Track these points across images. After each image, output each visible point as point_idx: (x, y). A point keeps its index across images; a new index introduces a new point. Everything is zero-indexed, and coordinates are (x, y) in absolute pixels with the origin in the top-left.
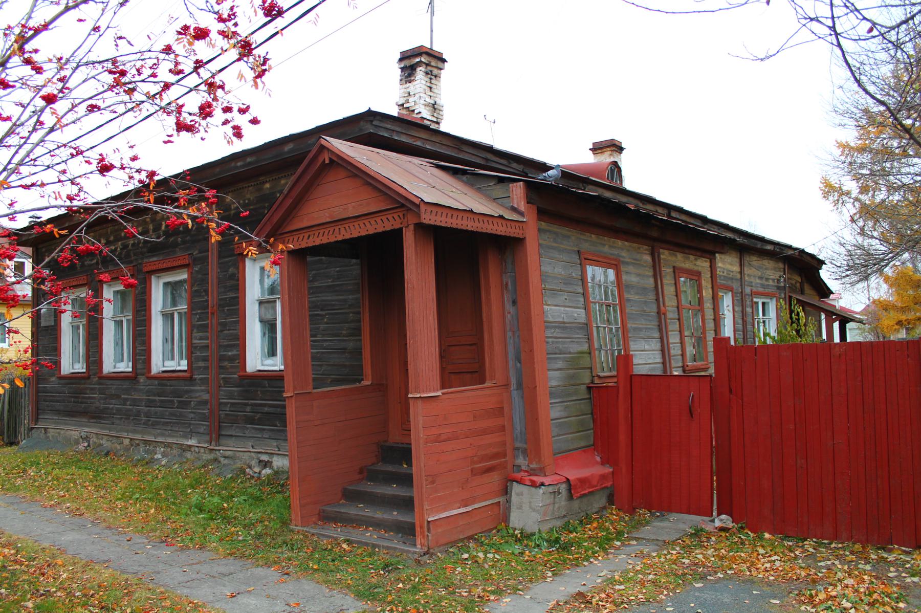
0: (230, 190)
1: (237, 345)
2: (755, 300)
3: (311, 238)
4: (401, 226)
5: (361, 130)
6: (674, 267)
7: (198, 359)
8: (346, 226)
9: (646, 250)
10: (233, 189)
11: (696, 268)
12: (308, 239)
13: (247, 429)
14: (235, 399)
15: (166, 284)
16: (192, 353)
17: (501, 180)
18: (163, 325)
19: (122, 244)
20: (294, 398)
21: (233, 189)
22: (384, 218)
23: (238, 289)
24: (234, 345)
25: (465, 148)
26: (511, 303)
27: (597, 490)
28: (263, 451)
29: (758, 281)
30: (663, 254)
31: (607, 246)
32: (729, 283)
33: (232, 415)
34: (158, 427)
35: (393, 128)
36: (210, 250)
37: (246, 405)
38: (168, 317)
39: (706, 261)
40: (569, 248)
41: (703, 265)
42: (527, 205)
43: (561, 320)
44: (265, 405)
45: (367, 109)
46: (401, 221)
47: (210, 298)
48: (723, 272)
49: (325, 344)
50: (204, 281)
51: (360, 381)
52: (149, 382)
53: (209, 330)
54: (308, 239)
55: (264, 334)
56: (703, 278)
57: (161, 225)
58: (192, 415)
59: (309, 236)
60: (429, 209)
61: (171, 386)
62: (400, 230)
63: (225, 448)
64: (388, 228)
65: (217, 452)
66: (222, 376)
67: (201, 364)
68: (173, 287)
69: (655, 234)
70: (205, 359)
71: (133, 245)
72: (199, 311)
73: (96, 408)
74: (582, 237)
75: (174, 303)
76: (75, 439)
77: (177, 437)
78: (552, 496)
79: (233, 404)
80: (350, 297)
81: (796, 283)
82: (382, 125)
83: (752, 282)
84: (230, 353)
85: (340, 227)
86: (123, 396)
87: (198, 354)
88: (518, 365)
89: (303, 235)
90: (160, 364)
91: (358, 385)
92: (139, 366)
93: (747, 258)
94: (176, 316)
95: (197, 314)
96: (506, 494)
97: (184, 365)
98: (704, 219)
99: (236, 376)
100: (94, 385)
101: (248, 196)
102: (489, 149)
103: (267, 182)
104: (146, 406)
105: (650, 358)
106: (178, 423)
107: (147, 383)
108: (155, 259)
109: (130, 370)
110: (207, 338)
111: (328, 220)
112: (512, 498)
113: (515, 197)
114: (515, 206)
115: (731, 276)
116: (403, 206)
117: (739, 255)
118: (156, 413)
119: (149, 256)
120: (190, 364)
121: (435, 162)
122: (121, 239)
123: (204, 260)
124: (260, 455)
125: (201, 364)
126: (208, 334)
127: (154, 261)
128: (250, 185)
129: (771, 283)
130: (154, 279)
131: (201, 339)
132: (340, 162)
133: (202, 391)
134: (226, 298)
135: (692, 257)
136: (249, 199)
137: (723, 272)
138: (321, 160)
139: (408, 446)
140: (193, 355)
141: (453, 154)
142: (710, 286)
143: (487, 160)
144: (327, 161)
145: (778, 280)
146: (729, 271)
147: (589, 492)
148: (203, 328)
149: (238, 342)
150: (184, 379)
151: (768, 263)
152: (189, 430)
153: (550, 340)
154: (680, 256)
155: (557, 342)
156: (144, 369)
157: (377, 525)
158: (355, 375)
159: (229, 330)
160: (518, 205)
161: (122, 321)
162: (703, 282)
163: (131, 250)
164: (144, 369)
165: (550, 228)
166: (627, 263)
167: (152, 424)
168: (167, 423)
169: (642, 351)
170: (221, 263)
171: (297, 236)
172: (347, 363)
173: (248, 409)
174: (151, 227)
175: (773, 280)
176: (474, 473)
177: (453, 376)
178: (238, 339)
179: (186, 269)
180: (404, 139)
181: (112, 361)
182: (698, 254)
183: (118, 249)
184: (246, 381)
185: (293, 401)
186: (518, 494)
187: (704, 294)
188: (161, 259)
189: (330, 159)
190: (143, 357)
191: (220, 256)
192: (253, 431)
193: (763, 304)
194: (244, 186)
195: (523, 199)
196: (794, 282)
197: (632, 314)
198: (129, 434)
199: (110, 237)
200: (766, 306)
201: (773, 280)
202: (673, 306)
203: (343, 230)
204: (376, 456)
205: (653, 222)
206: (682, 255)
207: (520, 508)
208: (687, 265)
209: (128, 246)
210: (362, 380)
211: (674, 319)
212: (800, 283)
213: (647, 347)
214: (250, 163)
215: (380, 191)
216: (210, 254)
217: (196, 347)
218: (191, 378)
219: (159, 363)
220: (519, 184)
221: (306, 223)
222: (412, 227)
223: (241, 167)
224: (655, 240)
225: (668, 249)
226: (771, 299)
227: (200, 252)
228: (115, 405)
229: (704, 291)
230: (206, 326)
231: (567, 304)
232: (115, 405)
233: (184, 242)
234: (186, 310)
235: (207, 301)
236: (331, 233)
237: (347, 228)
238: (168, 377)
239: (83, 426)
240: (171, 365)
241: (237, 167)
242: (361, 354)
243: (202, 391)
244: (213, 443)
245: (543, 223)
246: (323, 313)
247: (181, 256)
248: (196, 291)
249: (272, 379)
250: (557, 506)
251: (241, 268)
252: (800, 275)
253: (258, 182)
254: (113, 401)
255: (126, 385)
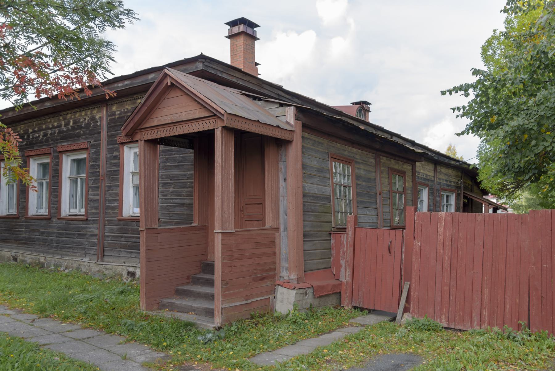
0: (115, 102)
1: (118, 200)
2: (442, 193)
3: (159, 133)
4: (214, 128)
5: (197, 67)
6: (388, 167)
7: (92, 208)
8: (181, 126)
9: (373, 156)
10: (117, 102)
11: (403, 169)
12: (157, 133)
13: (121, 251)
14: (115, 233)
15: (74, 161)
16: (88, 204)
17: (281, 105)
18: (70, 186)
19: (43, 133)
20: (145, 231)
21: (117, 102)
22: (204, 122)
23: (119, 165)
24: (116, 200)
25: (264, 86)
26: (283, 180)
27: (330, 294)
28: (131, 265)
29: (445, 182)
30: (382, 159)
31: (347, 152)
32: (427, 182)
33: (112, 243)
34: (64, 250)
35: (217, 68)
36: (101, 140)
37: (122, 237)
38: (74, 181)
39: (410, 166)
40: (322, 150)
41: (407, 168)
42: (295, 121)
43: (314, 192)
44: (133, 237)
45: (199, 54)
46: (213, 125)
47: (101, 170)
48: (423, 176)
49: (172, 201)
50: (97, 159)
51: (191, 223)
52: (59, 221)
53: (100, 190)
54: (157, 133)
55: (136, 194)
56: (407, 176)
57: (70, 122)
58: (87, 243)
59: (158, 131)
60: (230, 117)
61: (73, 224)
62: (214, 130)
63: (106, 263)
64: (206, 129)
65: (102, 266)
66: (107, 219)
67: (94, 211)
68: (79, 162)
69: (377, 146)
70: (96, 208)
71: (51, 134)
72: (94, 178)
73: (23, 237)
74: (331, 145)
75: (78, 173)
76: (8, 257)
77: (76, 256)
78: (302, 296)
79: (113, 236)
80: (189, 173)
81: (468, 185)
82: (211, 66)
83: (441, 183)
84: (113, 205)
85: (177, 126)
86: (41, 230)
87: (92, 205)
88: (286, 217)
89: (154, 130)
90: (67, 211)
91: (190, 225)
92: (53, 211)
93: (439, 168)
94: (79, 180)
95: (92, 179)
96: (274, 293)
97: (83, 211)
98: (413, 143)
99: (116, 219)
100: (22, 222)
101: (127, 107)
102: (280, 88)
103: (139, 98)
104: (57, 237)
105: (370, 220)
106: (77, 248)
107: (58, 222)
108: (65, 144)
109: (47, 214)
110: (98, 195)
111: (170, 122)
112: (278, 296)
113: (288, 115)
114: (288, 121)
115: (428, 178)
116: (215, 115)
117: (434, 166)
118: (63, 241)
119: (62, 142)
120: (87, 211)
121: (243, 92)
122: (42, 130)
123: (98, 146)
124: (128, 268)
125: (94, 211)
126: (99, 192)
127: (65, 145)
128: (128, 99)
129: (453, 184)
130: (64, 157)
131: (94, 195)
132: (177, 85)
133: (94, 228)
134: (112, 171)
135: (401, 163)
136: (127, 109)
137: (423, 176)
138: (165, 83)
139: (213, 263)
140: (89, 205)
141: (257, 89)
142: (411, 180)
143: (279, 95)
144: (169, 84)
145: (457, 183)
146: (427, 175)
147: (325, 295)
148: (94, 188)
149: (118, 198)
150: (82, 220)
151: (450, 171)
152: (84, 252)
153: (307, 203)
154: (393, 161)
155: (311, 205)
156: (56, 213)
157: (194, 310)
158: (189, 219)
159: (112, 190)
160: (290, 121)
161: (43, 183)
162: (407, 178)
163: (49, 137)
164: (56, 213)
165: (310, 137)
166: (359, 163)
167: (60, 248)
168: (70, 247)
169: (365, 215)
170: (109, 149)
171: (151, 131)
172: (185, 213)
173: (123, 239)
174: (63, 123)
175: (454, 182)
176: (254, 280)
177: (247, 222)
178: (118, 196)
179: (85, 152)
180: (225, 76)
181: (35, 208)
182: (405, 161)
183: (41, 136)
184: (122, 222)
185: (145, 233)
186: (281, 294)
187: (407, 185)
188: (69, 144)
189: (171, 83)
190: (56, 206)
191: (109, 143)
192: (125, 253)
193: (447, 196)
194: (125, 100)
195: (293, 117)
196: (467, 185)
197: (360, 193)
198: (45, 254)
199: (35, 128)
200: (449, 198)
201: (454, 182)
202: (386, 191)
203: (178, 129)
204: (199, 269)
205: (376, 139)
206: (394, 161)
207: (282, 302)
208: (397, 167)
209: (47, 134)
210: (193, 223)
211: (387, 198)
212: (471, 186)
213: (368, 213)
214: (127, 85)
215: (202, 105)
216: (101, 142)
217: (91, 201)
218: (87, 220)
219: (66, 210)
220: (291, 107)
221: (155, 124)
222: (220, 129)
223: (121, 87)
224: (377, 150)
225: (386, 157)
226: (452, 193)
227: (95, 141)
228: (36, 236)
229: (407, 183)
230: (98, 187)
231: (319, 184)
232: (36, 236)
233: (85, 134)
234: (85, 177)
235: (99, 172)
236: (171, 130)
237: (181, 127)
238: (73, 218)
239: (13, 248)
240: (74, 211)
241: (118, 87)
242: (192, 207)
243: (94, 228)
244: (99, 260)
245: (306, 134)
246: (172, 181)
247: (82, 143)
248: (92, 165)
249: (134, 220)
250: (304, 302)
251: (121, 152)
252: (472, 181)
253: (134, 98)
254: (35, 233)
255: (44, 223)
